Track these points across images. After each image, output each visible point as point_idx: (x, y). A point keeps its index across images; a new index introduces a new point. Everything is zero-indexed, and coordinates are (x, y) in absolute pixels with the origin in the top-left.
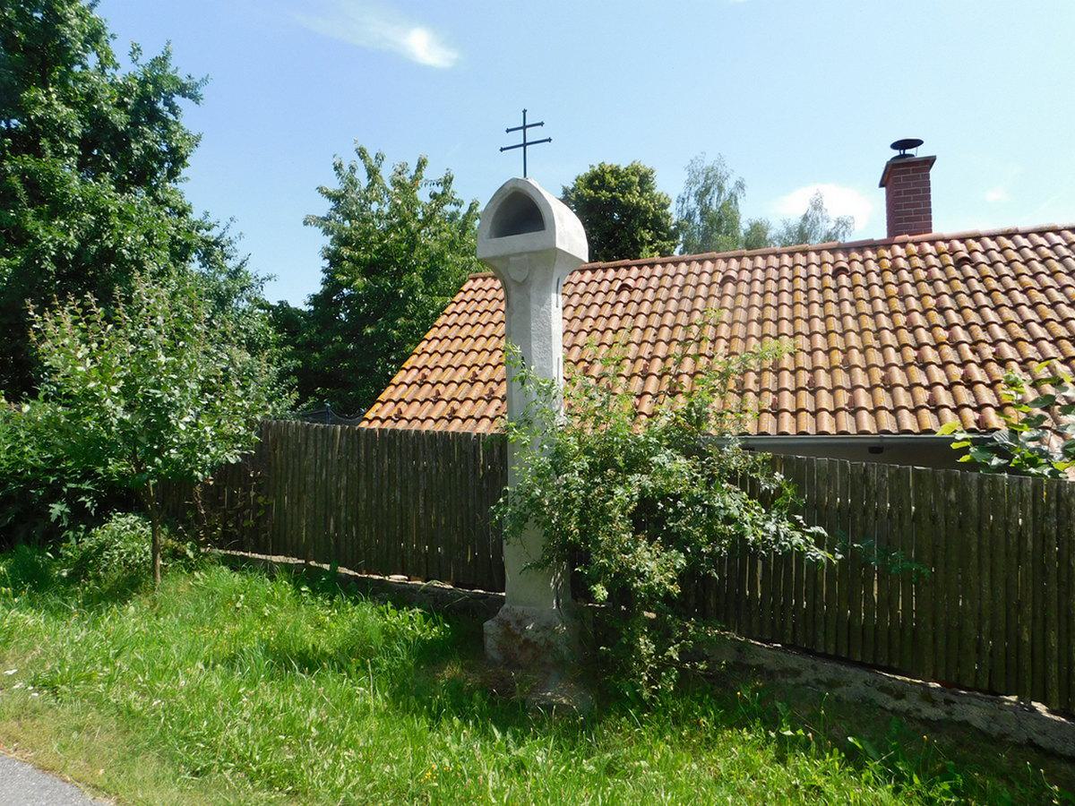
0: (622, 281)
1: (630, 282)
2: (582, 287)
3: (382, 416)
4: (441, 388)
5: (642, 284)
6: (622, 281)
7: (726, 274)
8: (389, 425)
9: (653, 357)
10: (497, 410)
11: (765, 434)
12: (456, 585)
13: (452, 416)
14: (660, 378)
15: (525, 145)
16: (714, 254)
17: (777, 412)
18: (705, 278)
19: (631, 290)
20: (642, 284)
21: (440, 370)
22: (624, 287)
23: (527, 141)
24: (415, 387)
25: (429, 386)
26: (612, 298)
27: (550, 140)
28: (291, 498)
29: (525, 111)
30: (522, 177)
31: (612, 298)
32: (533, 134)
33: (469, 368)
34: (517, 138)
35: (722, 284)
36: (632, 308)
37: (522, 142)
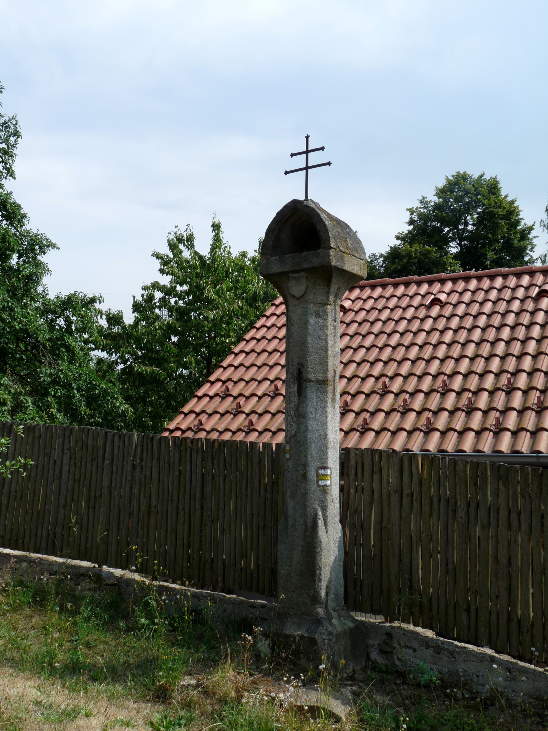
0: (435, 295)
1: (443, 297)
2: (393, 302)
3: (183, 427)
4: (242, 401)
5: (454, 298)
6: (435, 295)
7: (542, 288)
8: (240, 437)
9: (518, 371)
10: (178, 424)
11: (518, 452)
12: (437, 634)
13: (251, 429)
14: (397, 395)
15: (307, 168)
16: (443, 275)
17: (499, 431)
18: (520, 293)
19: (442, 305)
20: (454, 298)
21: (243, 383)
22: (436, 301)
23: (309, 165)
24: (218, 399)
25: (231, 399)
26: (422, 313)
27: (329, 164)
28: (88, 501)
29: (307, 137)
30: (302, 197)
31: (422, 313)
32: (314, 159)
33: (272, 382)
34: (300, 162)
35: (429, 307)
36: (441, 324)
37: (304, 166)
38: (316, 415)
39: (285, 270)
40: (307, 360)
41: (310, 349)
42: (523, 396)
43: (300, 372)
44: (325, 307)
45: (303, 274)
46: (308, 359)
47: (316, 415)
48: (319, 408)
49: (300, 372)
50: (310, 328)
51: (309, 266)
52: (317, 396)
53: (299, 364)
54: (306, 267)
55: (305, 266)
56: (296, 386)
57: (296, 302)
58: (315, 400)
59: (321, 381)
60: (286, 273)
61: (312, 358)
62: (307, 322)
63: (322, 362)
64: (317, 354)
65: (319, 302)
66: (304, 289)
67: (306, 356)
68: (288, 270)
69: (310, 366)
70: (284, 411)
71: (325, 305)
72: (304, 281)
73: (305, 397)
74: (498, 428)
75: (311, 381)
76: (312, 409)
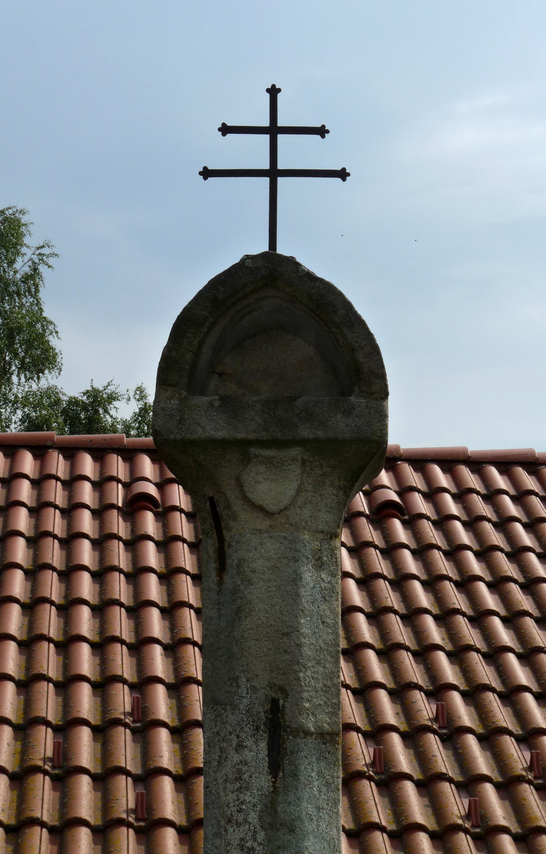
38: (318, 825)
39: (240, 436)
40: (298, 679)
41: (307, 651)
42: (16, 739)
43: (275, 710)
44: (332, 543)
45: (295, 452)
46: (301, 675)
47: (318, 825)
48: (325, 806)
49: (275, 710)
50: (306, 593)
51: (321, 434)
52: (320, 774)
53: (271, 686)
54: (312, 436)
55: (306, 432)
56: (263, 745)
57: (264, 524)
58: (316, 784)
59: (328, 734)
60: (243, 445)
61: (309, 673)
62: (296, 579)
63: (329, 683)
64: (318, 663)
65: (321, 527)
66: (293, 492)
67: (296, 667)
68: (251, 437)
69: (305, 695)
70: (467, 825)
71: (331, 538)
72: (295, 470)
73: (295, 775)
74: (144, 820)
75: (307, 733)
76: (311, 809)
